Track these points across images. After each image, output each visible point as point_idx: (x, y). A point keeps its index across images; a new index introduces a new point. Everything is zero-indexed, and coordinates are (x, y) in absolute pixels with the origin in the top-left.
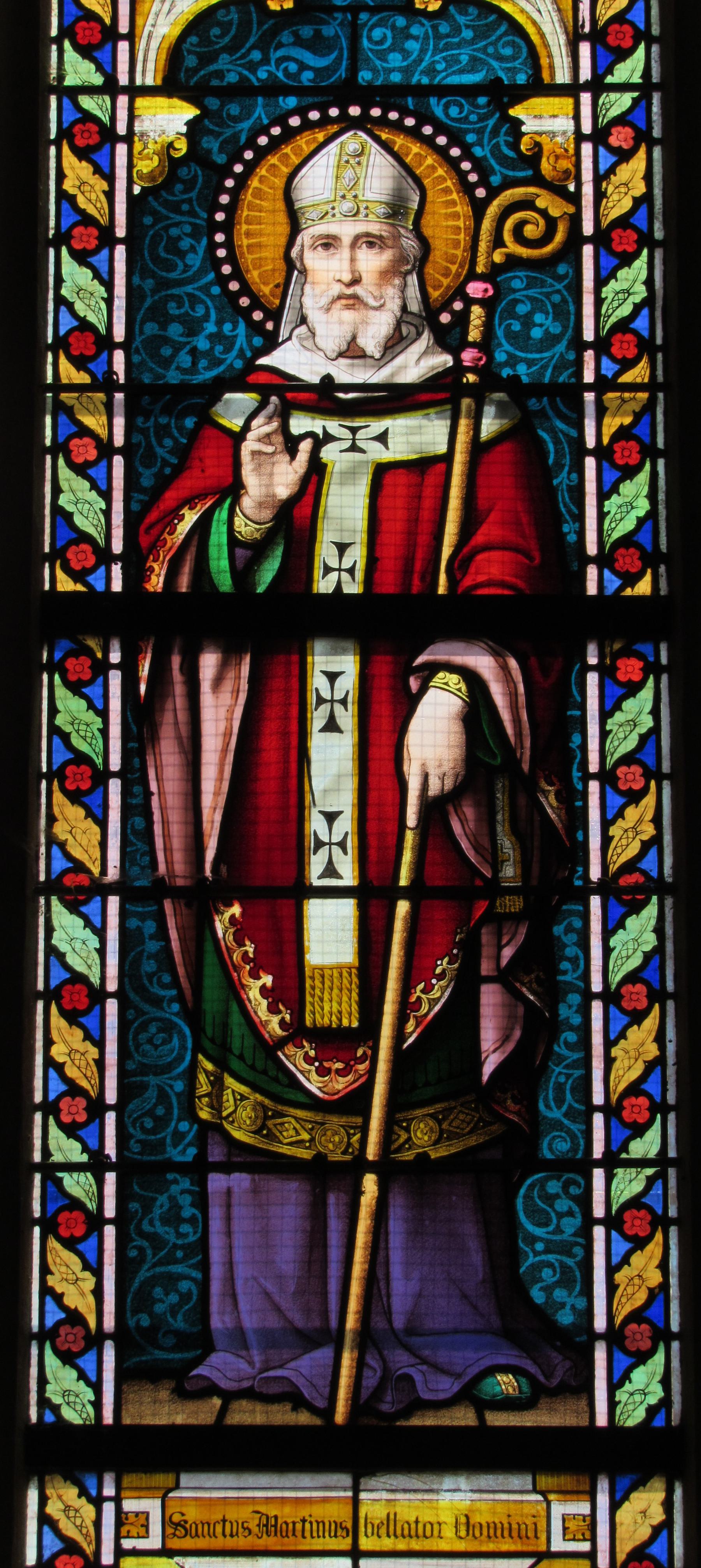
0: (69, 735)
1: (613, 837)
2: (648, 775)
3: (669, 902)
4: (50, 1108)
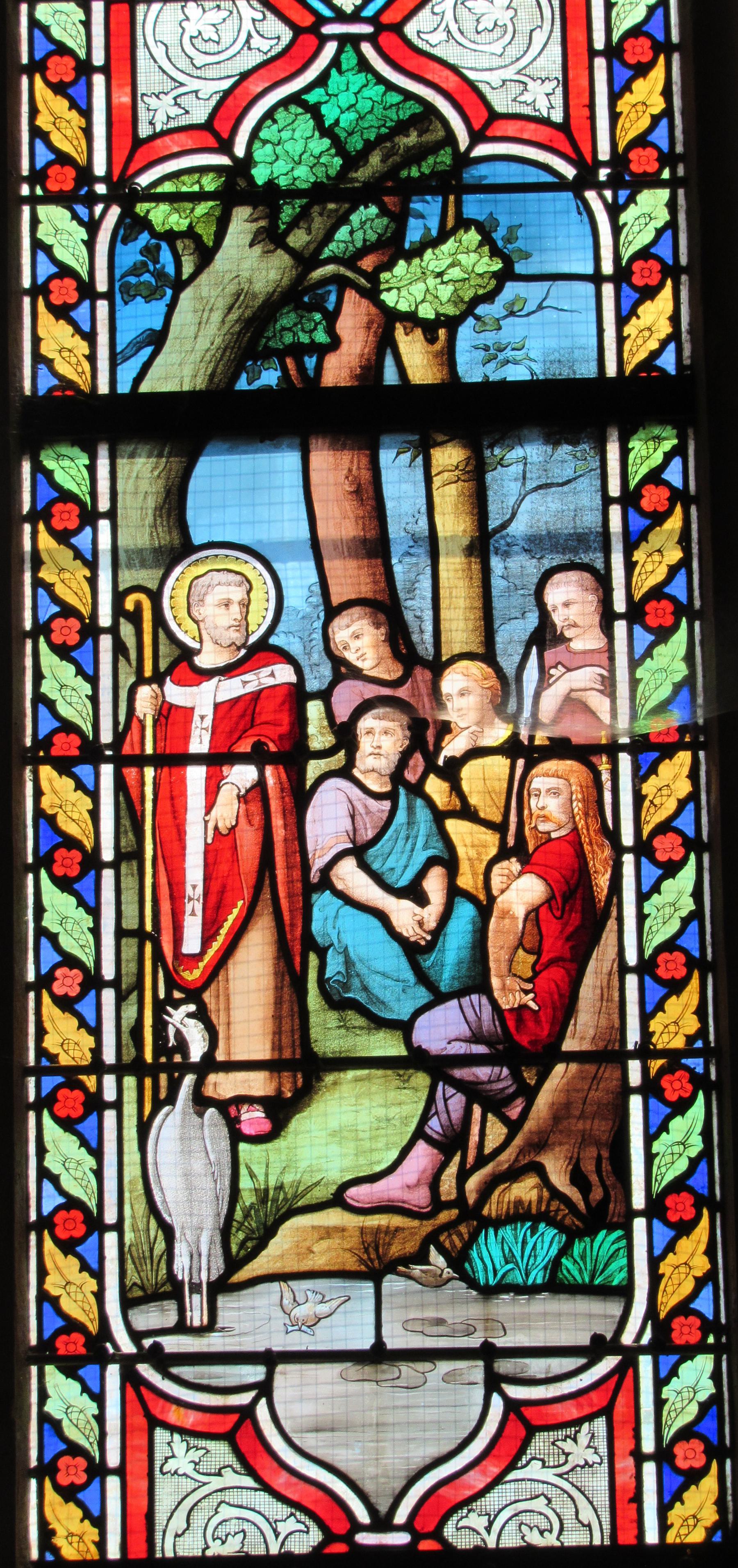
0: (58, 1298)
2: (700, 1202)
4: (39, 290)
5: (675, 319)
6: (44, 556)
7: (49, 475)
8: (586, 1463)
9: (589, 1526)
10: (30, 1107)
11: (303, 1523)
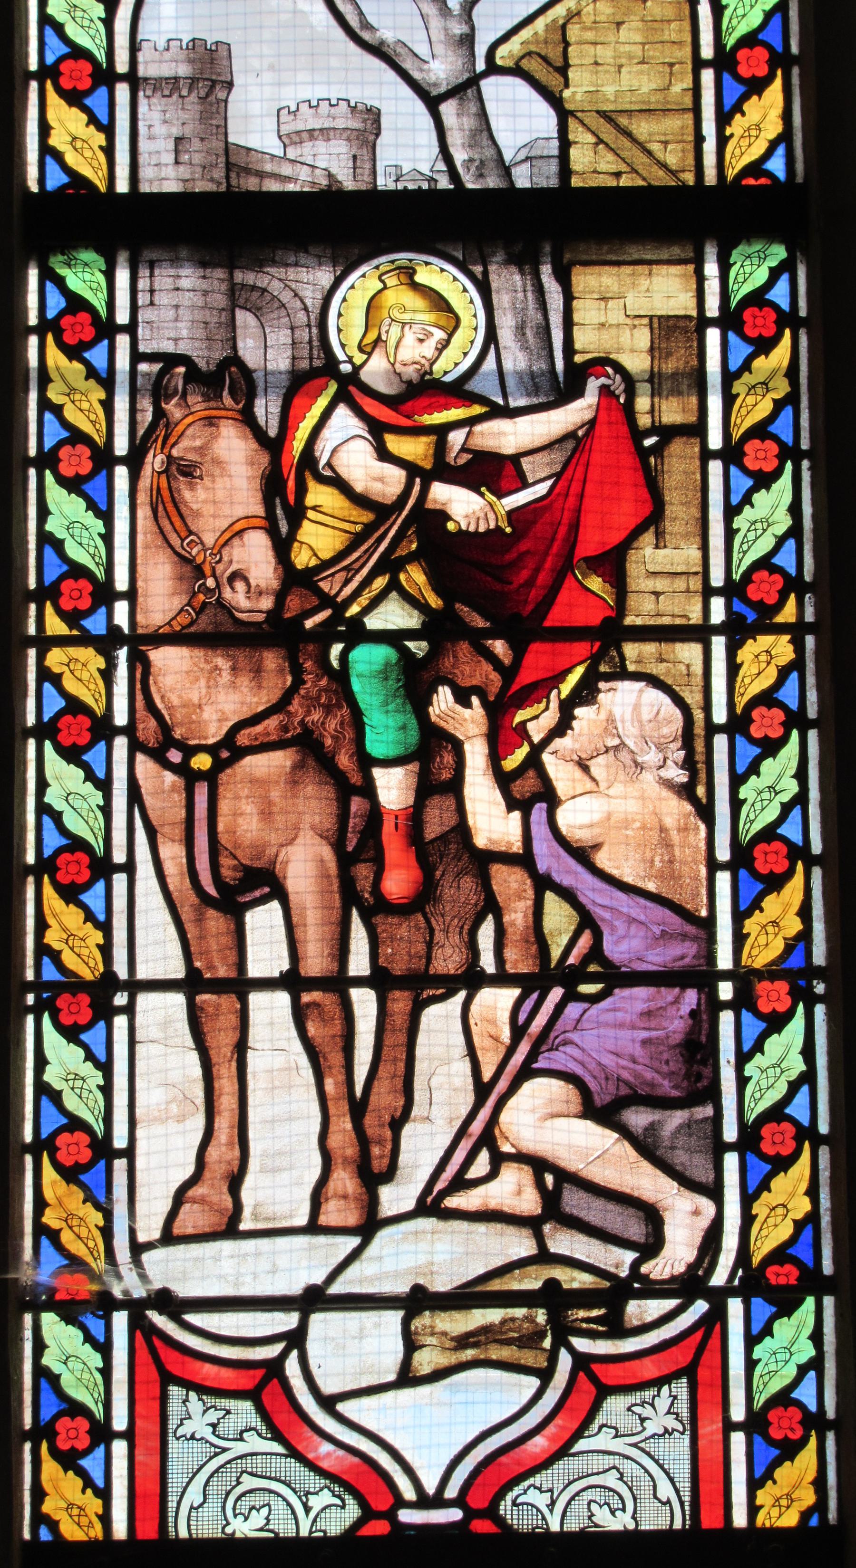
0: (60, 676)
1: (748, 935)
3: (829, 1302)
5: (795, 509)
6: (53, 374)
7: (60, 283)
8: (666, 1431)
9: (668, 1502)
10: (27, 1436)
11: (339, 1497)
